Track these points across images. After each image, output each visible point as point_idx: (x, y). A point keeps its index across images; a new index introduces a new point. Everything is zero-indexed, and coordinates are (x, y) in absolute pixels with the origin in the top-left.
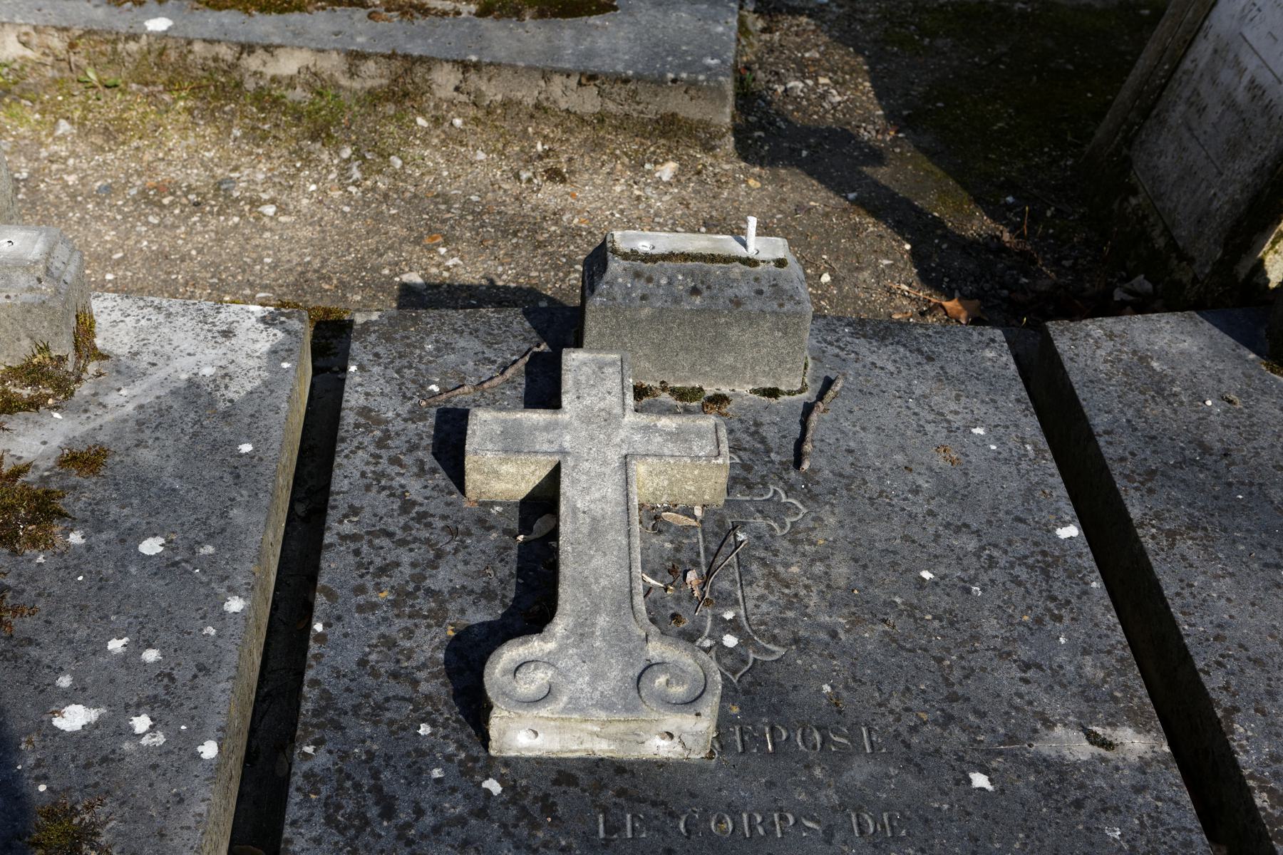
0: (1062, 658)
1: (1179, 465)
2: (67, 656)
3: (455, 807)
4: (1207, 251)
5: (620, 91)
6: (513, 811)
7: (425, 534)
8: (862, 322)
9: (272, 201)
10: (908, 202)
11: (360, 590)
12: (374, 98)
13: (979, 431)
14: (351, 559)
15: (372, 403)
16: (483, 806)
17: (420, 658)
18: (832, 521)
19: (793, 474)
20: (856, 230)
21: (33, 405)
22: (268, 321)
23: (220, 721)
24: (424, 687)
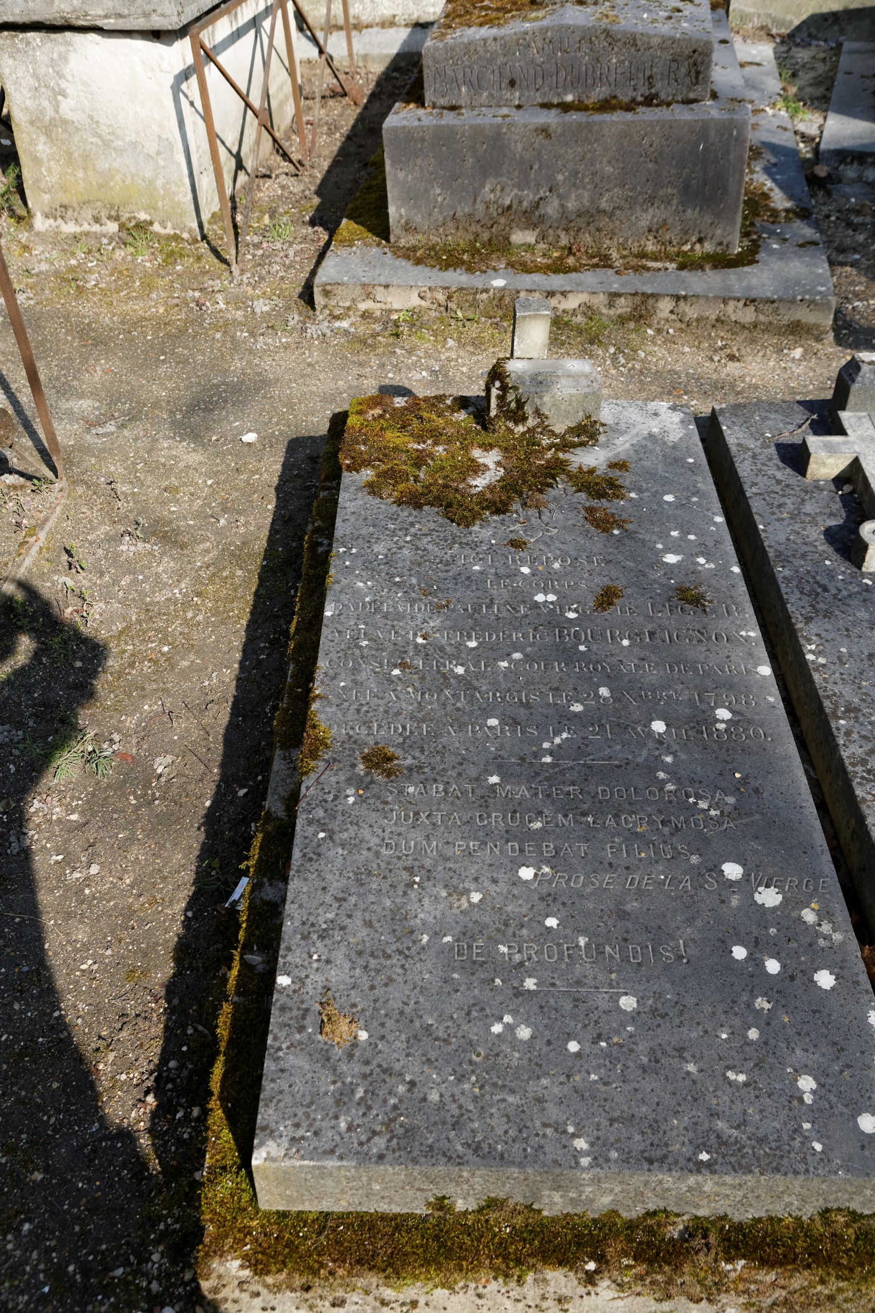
5: (768, 308)
7: (793, 492)
11: (773, 513)
12: (622, 320)
15: (740, 441)
21: (582, 444)
24: (820, 548)
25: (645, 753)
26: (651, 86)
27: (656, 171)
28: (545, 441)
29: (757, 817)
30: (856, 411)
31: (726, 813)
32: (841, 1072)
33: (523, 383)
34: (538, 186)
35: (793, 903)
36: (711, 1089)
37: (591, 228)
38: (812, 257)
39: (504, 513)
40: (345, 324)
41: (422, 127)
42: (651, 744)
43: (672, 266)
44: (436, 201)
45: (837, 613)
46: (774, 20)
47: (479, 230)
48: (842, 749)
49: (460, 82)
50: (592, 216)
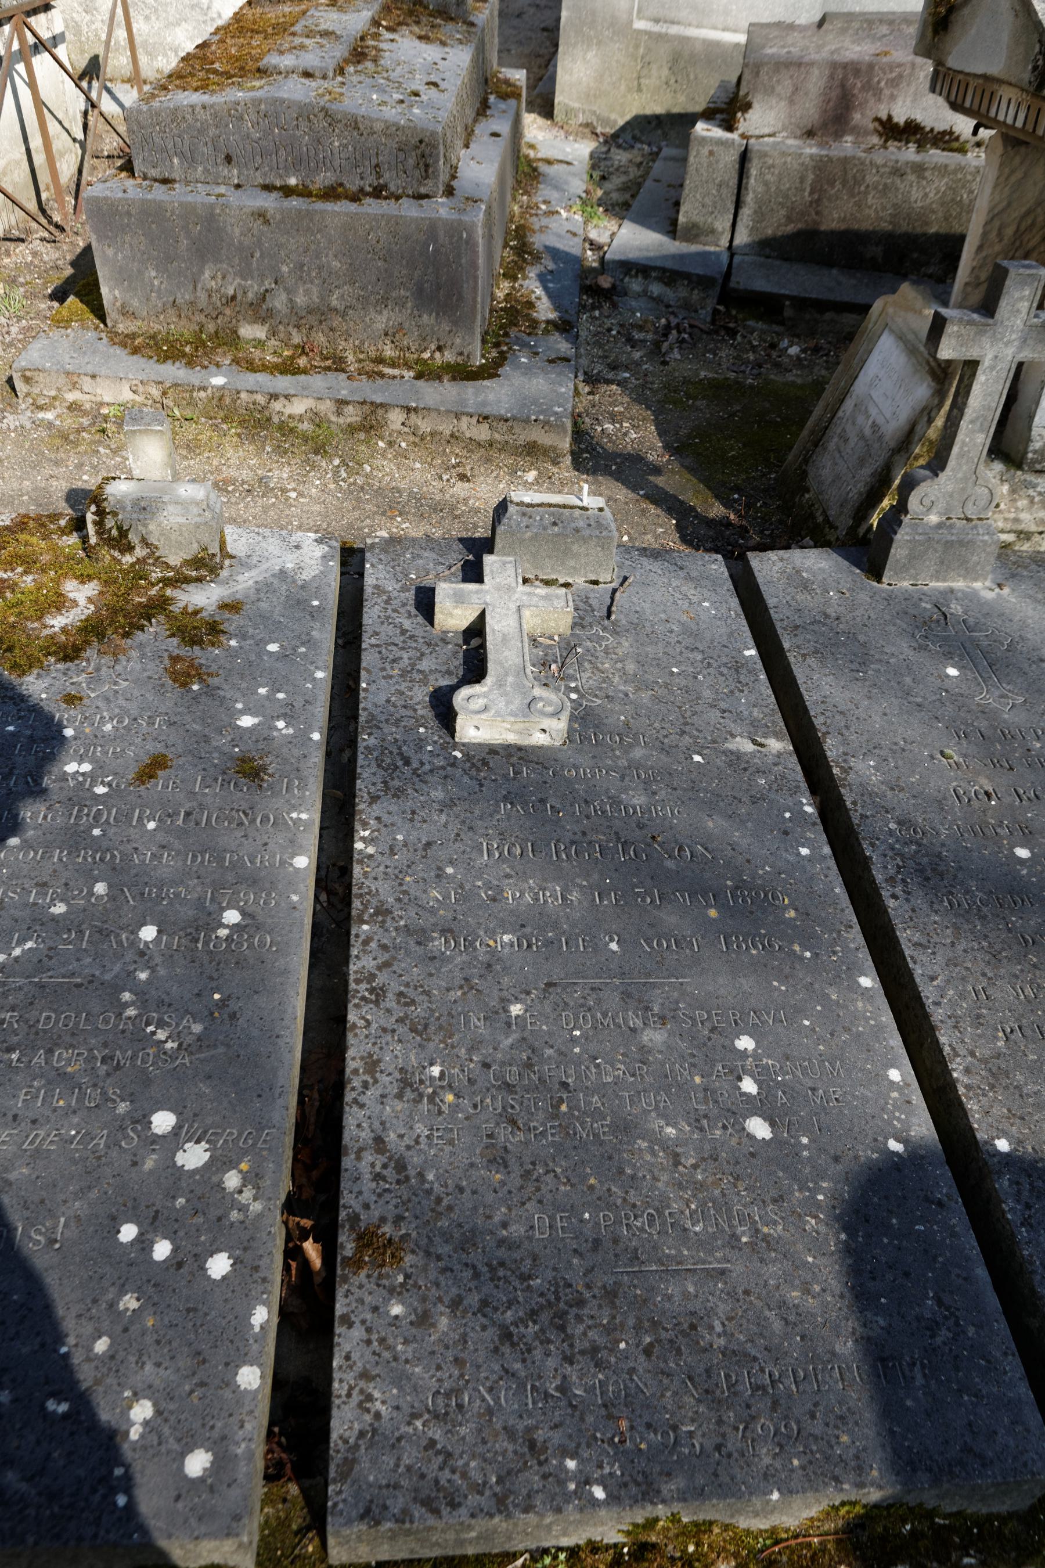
0: (742, 708)
1: (812, 623)
2: (238, 695)
3: (439, 762)
4: (844, 522)
5: (503, 427)
6: (468, 765)
7: (414, 645)
8: (645, 549)
9: (294, 490)
10: (675, 497)
11: (384, 669)
12: (351, 430)
13: (706, 604)
14: (377, 655)
15: (379, 583)
16: (454, 763)
17: (416, 700)
18: (626, 644)
19: (606, 622)
20: (644, 512)
21: (199, 580)
22: (319, 541)
23: (320, 724)
24: (420, 712)
25: (117, 967)
26: (379, 176)
27: (386, 271)
28: (156, 574)
29: (221, 1050)
30: (504, 555)
31: (184, 1046)
32: (192, 1392)
33: (124, 508)
34: (262, 277)
35: (218, 1164)
36: (18, 1426)
37: (324, 326)
38: (559, 374)
39: (72, 660)
40: (49, 416)
41: (127, 200)
42: (130, 956)
43: (409, 374)
44: (152, 285)
45: (410, 791)
46: (598, 118)
47: (204, 320)
48: (353, 960)
49: (171, 152)
50: (323, 314)
